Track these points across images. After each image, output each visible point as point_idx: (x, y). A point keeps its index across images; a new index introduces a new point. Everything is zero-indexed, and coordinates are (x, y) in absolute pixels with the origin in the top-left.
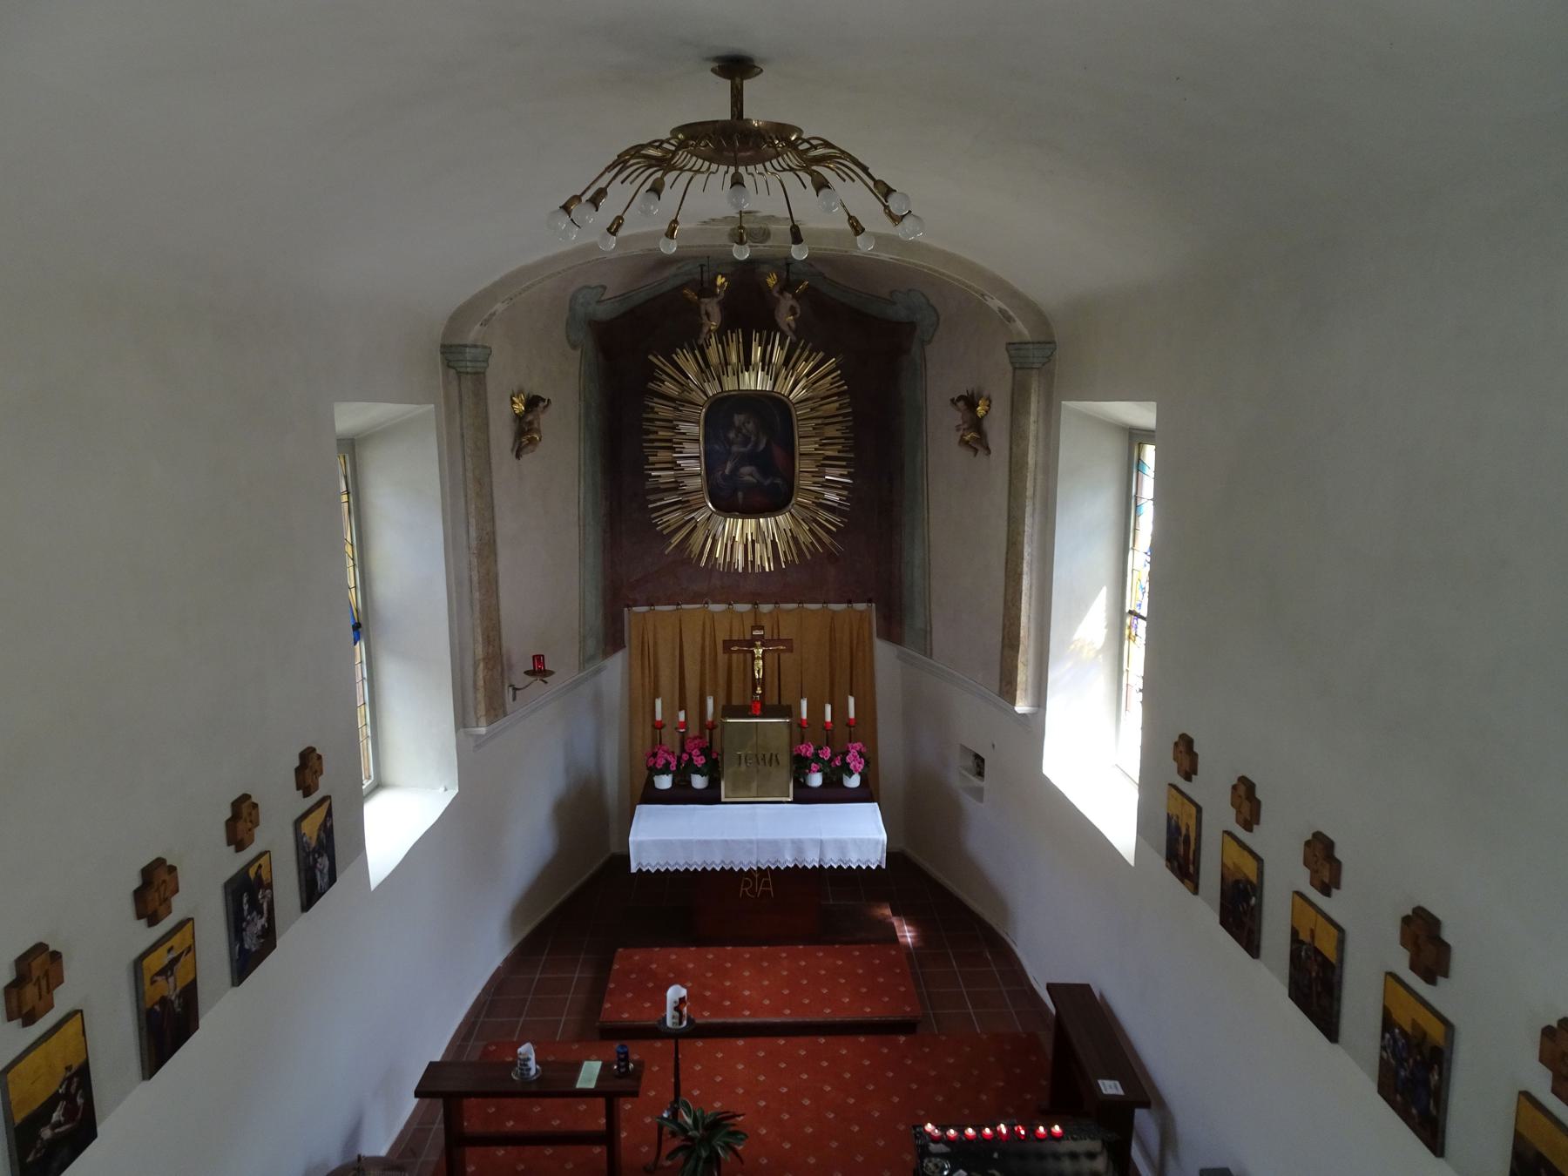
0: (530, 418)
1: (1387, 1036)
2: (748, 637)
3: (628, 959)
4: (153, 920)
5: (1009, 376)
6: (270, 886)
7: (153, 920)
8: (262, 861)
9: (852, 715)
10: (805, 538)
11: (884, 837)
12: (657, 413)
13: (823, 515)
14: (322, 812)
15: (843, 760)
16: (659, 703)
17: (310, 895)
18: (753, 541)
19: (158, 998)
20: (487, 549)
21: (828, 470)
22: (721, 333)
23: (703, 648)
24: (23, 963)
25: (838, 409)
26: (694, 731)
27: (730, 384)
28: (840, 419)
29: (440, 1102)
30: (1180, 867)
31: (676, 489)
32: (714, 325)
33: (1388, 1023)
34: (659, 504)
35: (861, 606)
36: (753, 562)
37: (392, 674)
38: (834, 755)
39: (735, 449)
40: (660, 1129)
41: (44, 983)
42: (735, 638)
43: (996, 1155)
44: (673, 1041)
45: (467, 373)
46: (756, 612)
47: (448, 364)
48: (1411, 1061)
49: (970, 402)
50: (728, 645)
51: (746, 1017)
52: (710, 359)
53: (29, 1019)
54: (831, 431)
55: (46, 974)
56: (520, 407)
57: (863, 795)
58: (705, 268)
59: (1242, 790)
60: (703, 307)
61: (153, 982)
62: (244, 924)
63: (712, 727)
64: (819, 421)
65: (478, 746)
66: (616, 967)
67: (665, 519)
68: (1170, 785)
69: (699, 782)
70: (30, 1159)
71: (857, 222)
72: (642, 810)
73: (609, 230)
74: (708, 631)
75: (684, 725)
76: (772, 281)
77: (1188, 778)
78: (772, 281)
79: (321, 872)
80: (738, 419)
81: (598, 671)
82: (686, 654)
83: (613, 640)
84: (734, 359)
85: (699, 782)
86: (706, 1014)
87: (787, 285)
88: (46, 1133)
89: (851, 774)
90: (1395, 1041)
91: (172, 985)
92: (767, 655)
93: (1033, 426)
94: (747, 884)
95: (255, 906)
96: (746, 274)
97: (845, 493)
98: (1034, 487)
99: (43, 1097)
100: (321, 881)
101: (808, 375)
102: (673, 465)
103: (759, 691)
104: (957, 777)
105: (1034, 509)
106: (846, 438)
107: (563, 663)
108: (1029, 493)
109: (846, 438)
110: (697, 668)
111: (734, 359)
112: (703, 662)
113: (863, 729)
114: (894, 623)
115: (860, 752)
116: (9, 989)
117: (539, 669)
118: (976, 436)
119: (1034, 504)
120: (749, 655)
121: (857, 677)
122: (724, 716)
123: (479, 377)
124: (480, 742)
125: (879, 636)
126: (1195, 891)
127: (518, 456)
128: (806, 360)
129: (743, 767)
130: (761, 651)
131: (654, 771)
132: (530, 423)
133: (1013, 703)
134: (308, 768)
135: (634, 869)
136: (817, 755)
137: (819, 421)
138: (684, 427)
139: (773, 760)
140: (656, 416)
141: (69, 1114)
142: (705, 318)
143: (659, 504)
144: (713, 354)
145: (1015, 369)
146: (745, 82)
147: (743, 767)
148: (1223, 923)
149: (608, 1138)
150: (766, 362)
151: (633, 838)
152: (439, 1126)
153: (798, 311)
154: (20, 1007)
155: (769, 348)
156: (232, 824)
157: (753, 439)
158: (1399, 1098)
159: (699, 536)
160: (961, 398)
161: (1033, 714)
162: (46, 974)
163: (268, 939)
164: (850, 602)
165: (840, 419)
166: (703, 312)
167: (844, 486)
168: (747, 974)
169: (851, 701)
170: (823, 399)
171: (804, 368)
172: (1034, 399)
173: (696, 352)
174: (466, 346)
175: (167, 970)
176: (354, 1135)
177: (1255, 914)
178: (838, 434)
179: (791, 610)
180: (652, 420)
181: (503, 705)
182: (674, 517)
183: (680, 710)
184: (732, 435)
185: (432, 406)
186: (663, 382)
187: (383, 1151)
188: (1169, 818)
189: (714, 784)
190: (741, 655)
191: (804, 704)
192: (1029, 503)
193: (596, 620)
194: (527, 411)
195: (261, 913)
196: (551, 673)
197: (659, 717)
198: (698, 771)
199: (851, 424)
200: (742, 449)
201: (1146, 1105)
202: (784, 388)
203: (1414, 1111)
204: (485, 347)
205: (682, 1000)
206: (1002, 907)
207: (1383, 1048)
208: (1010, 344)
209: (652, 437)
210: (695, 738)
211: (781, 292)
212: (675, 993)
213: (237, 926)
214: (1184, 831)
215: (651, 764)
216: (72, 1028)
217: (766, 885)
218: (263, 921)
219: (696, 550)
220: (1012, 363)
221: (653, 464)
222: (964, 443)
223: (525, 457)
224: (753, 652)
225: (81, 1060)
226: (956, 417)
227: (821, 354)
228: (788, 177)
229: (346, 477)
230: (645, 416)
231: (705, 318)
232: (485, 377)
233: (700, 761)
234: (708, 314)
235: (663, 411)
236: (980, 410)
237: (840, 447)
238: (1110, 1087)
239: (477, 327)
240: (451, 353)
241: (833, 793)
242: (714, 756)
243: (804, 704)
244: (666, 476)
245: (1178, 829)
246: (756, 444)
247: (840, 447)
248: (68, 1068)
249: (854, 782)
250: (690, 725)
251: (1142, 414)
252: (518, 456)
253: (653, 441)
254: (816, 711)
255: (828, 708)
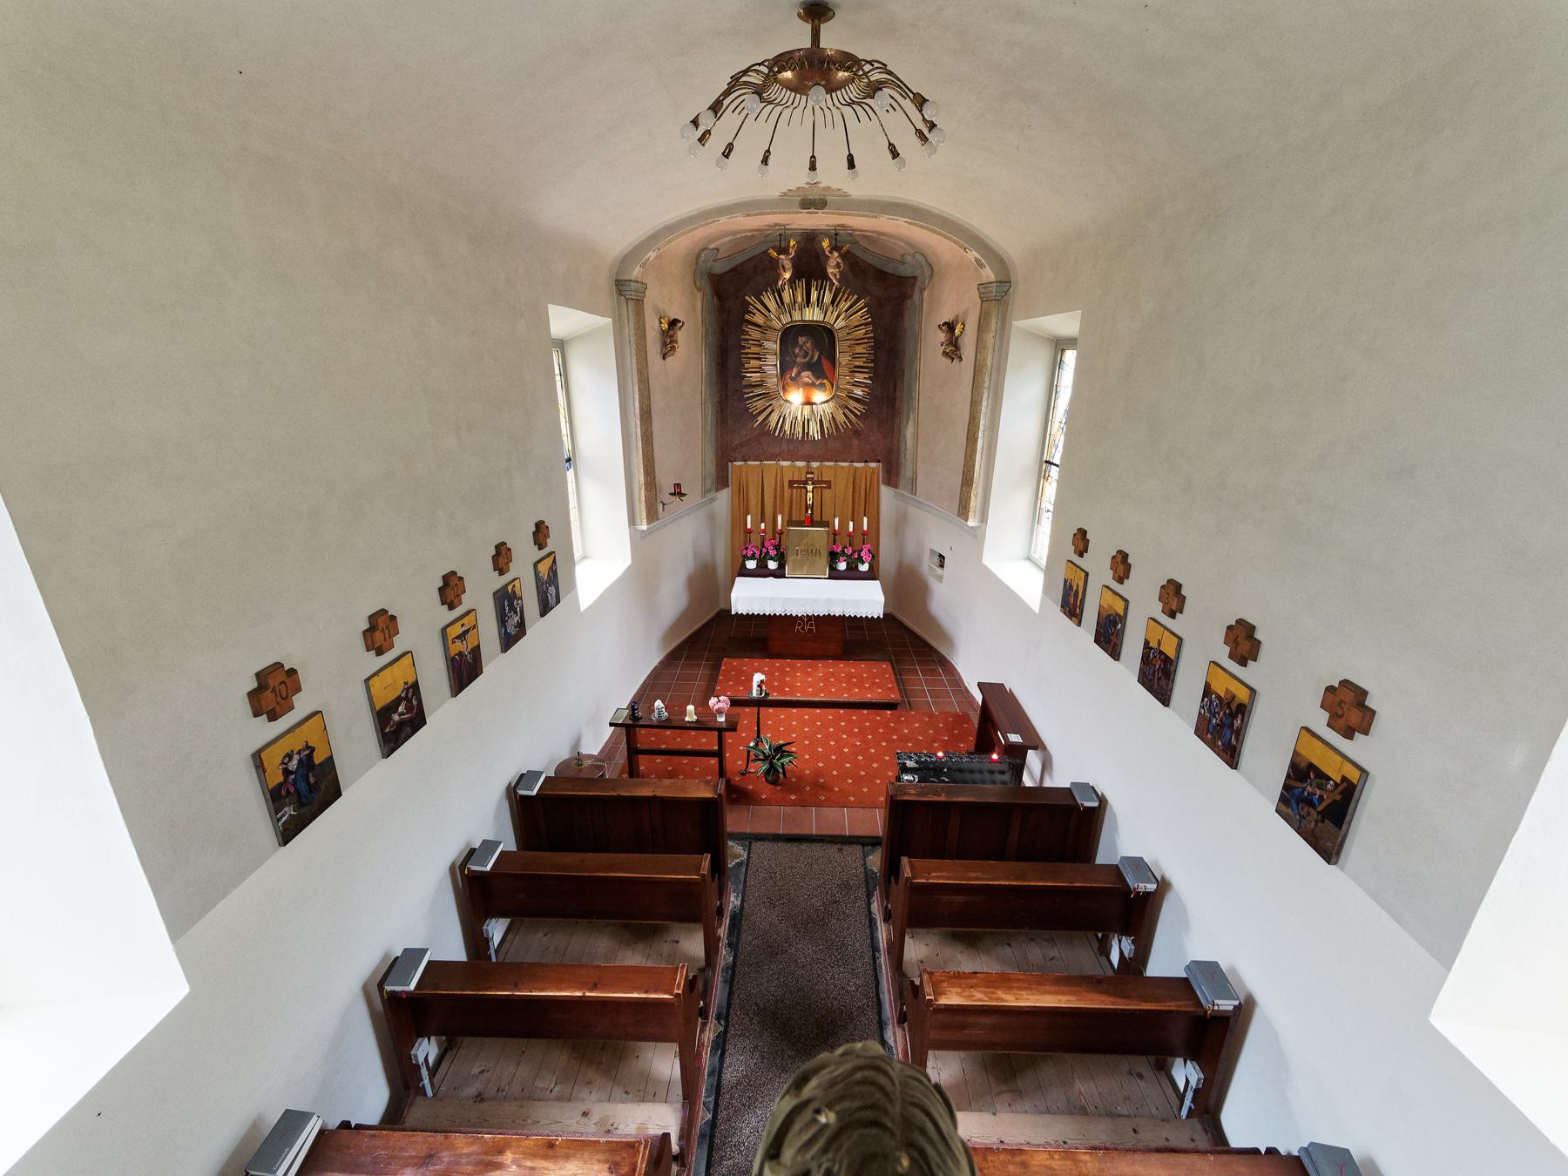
0: (671, 333)
1: (1206, 699)
2: (803, 479)
3: (729, 664)
4: (451, 607)
5: (979, 306)
6: (521, 598)
7: (451, 607)
8: (515, 583)
9: (865, 528)
10: (841, 418)
11: (882, 598)
12: (750, 335)
13: (852, 404)
14: (549, 561)
15: (859, 554)
16: (749, 517)
17: (545, 609)
18: (808, 420)
19: (457, 652)
20: (646, 416)
21: (856, 375)
22: (792, 281)
23: (776, 488)
24: (373, 618)
25: (865, 334)
26: (769, 535)
27: (797, 316)
28: (866, 340)
29: (624, 728)
30: (1070, 612)
31: (761, 385)
32: (787, 275)
33: (1207, 691)
34: (751, 395)
35: (873, 465)
36: (808, 433)
37: (589, 488)
38: (854, 552)
39: (798, 359)
40: (749, 752)
41: (386, 632)
42: (795, 479)
43: (945, 770)
44: (756, 709)
45: (632, 299)
46: (808, 466)
47: (620, 293)
48: (1222, 713)
49: (950, 327)
50: (791, 483)
51: (799, 697)
52: (784, 300)
53: (380, 652)
54: (859, 349)
55: (388, 627)
56: (665, 326)
57: (871, 575)
58: (782, 238)
59: (1119, 558)
60: (780, 262)
61: (453, 642)
62: (506, 618)
63: (781, 533)
64: (852, 342)
65: (642, 537)
66: (723, 668)
67: (754, 404)
68: (1069, 561)
69: (772, 565)
70: (387, 730)
71: (895, 148)
72: (739, 580)
73: (723, 154)
74: (779, 477)
75: (764, 531)
76: (825, 244)
77: (1081, 555)
78: (825, 244)
79: (551, 595)
80: (801, 340)
81: (713, 500)
82: (765, 492)
83: (722, 481)
84: (800, 300)
85: (772, 565)
86: (775, 694)
87: (834, 248)
88: (396, 717)
89: (863, 563)
90: (1211, 702)
91: (465, 646)
92: (815, 490)
93: (990, 339)
94: (800, 625)
95: (512, 608)
96: (810, 239)
97: (867, 390)
98: (990, 380)
99: (392, 696)
100: (552, 601)
101: (846, 311)
102: (760, 370)
103: (810, 512)
104: (927, 566)
105: (989, 396)
106: (868, 354)
107: (692, 488)
108: (986, 385)
109: (868, 354)
110: (772, 500)
111: (800, 300)
112: (775, 497)
113: (871, 537)
114: (892, 475)
115: (869, 550)
116: (365, 632)
117: (678, 492)
118: (953, 349)
119: (989, 393)
120: (804, 490)
121: (870, 506)
122: (788, 526)
123: (639, 303)
124: (644, 535)
125: (883, 483)
126: (1079, 624)
127: (664, 358)
128: (845, 301)
129: (799, 557)
130: (811, 487)
131: (746, 558)
132: (671, 336)
133: (967, 519)
134: (540, 533)
135: (733, 613)
136: (844, 551)
137: (852, 342)
138: (767, 344)
139: (817, 553)
140: (749, 337)
141: (409, 709)
142: (781, 269)
143: (751, 395)
144: (786, 295)
145: (982, 301)
146: (821, 25)
147: (799, 557)
148: (1096, 641)
149: (719, 754)
150: (820, 301)
151: (733, 595)
152: (624, 745)
153: (842, 265)
154: (373, 644)
155: (822, 292)
156: (496, 558)
157: (810, 353)
158: (1209, 736)
159: (774, 417)
160: (945, 324)
161: (979, 527)
162: (388, 627)
163: (521, 629)
164: (866, 462)
165: (866, 340)
166: (780, 265)
167: (866, 385)
168: (799, 674)
169: (865, 519)
170: (855, 327)
171: (844, 306)
172: (994, 321)
173: (776, 294)
174: (631, 281)
175: (462, 636)
176: (577, 743)
177: (1120, 635)
178: (864, 351)
179: (831, 466)
180: (747, 340)
181: (657, 513)
182: (760, 404)
183: (762, 522)
184: (797, 351)
185: (611, 320)
186: (754, 314)
187: (595, 752)
188: (1065, 581)
189: (782, 566)
190: (799, 490)
191: (837, 521)
192: (986, 391)
193: (711, 467)
194: (669, 329)
195: (516, 613)
196: (685, 495)
197: (749, 526)
198: (771, 559)
199: (872, 344)
200: (804, 360)
201: (1035, 748)
202: (830, 318)
203: (1220, 743)
204: (642, 283)
205: (762, 681)
206: (948, 640)
207: (1202, 707)
208: (979, 285)
209: (747, 351)
210: (770, 540)
211: (831, 252)
212: (758, 677)
213: (502, 620)
214: (1075, 588)
215: (744, 554)
216: (407, 660)
217: (811, 625)
218: (518, 618)
219: (773, 424)
220: (981, 298)
221: (747, 369)
222: (945, 354)
223: (669, 359)
224: (806, 488)
225: (413, 680)
226: (942, 336)
227: (856, 297)
228: (847, 110)
229: (559, 365)
230: (743, 337)
231: (781, 269)
232: (643, 304)
233: (773, 553)
234: (783, 267)
235: (754, 334)
236: (957, 332)
237: (865, 359)
238: (1015, 738)
239: (638, 267)
240: (621, 286)
241: (852, 574)
242: (782, 550)
243: (837, 521)
244: (755, 377)
245: (1071, 587)
246: (812, 356)
247: (865, 359)
248: (406, 683)
249: (864, 568)
250: (767, 531)
251: (1066, 324)
252: (664, 358)
253: (747, 354)
254: (843, 525)
255: (851, 524)
